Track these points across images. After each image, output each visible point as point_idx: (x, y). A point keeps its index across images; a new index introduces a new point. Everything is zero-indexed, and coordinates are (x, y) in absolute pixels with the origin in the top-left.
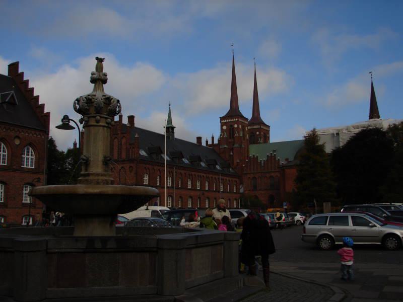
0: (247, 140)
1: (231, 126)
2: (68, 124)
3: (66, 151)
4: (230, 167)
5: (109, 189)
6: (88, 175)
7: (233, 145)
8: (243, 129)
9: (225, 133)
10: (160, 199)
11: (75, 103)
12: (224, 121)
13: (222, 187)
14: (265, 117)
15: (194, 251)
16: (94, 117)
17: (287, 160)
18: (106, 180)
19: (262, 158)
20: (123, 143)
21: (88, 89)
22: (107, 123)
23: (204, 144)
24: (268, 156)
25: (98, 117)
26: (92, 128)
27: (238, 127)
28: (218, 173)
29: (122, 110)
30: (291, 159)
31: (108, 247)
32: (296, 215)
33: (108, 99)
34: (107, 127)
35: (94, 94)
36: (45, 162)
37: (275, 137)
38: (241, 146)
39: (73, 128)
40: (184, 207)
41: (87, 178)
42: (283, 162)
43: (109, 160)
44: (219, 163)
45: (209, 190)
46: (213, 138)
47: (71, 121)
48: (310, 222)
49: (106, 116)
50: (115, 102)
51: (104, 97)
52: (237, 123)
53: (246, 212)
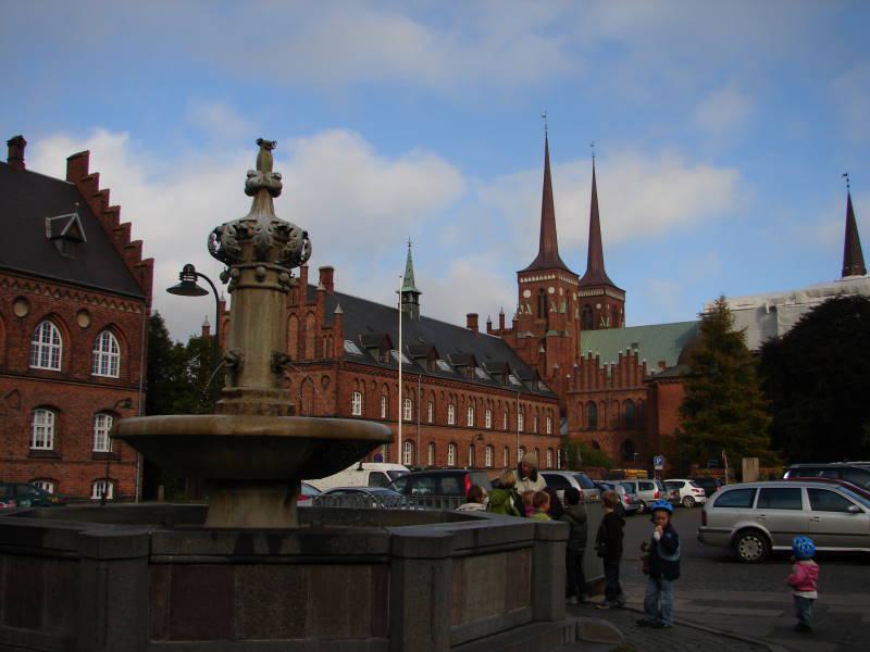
0: (576, 320)
2: (193, 283)
3: (186, 343)
4: (540, 379)
5: (285, 426)
6: (239, 394)
7: (547, 331)
8: (569, 299)
9: (528, 306)
11: (211, 238)
12: (526, 280)
13: (520, 421)
14: (614, 272)
15: (470, 563)
16: (254, 268)
17: (662, 364)
18: (278, 406)
19: (609, 361)
20: (308, 328)
21: (239, 207)
22: (280, 281)
23: (482, 329)
25: (262, 270)
26: (247, 291)
27: (557, 292)
28: (512, 392)
30: (672, 362)
31: (283, 552)
32: (682, 485)
33: (284, 231)
34: (280, 290)
35: (254, 218)
37: (636, 315)
38: (563, 332)
39: (206, 293)
40: (460, 466)
41: (235, 401)
42: (653, 369)
43: (284, 363)
44: (514, 371)
45: (492, 430)
46: (502, 317)
47: (199, 278)
48: (717, 501)
49: (279, 267)
50: (299, 237)
51: (275, 226)
52: (555, 283)
53: (574, 477)
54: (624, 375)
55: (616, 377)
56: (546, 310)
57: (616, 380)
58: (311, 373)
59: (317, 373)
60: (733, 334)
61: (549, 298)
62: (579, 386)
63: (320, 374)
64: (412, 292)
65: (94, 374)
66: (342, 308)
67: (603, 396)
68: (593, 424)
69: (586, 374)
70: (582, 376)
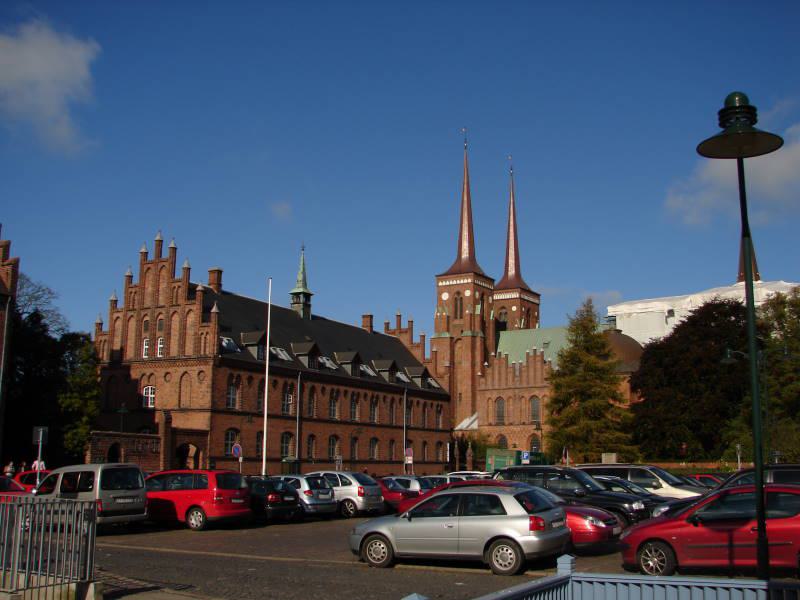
1: (458, 293)
12: (444, 283)
20: (188, 326)
24: (528, 354)
32: (347, 483)
48: (522, 494)
54: (532, 374)
56: (462, 311)
57: (524, 378)
59: (195, 368)
60: (599, 336)
61: (465, 302)
62: (489, 382)
63: (196, 369)
64: (303, 293)
65: (61, 368)
66: (219, 308)
67: (510, 393)
68: (500, 420)
69: (496, 372)
70: (493, 374)
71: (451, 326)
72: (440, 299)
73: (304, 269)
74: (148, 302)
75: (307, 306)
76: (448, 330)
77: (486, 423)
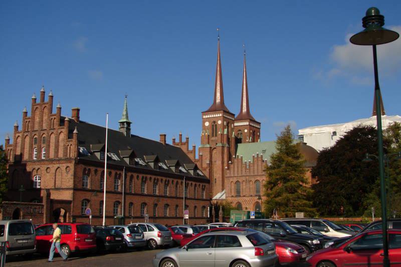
10: (197, 235)
12: (206, 117)
29: (22, 120)
32: (151, 230)
36: (88, 246)
46: (181, 135)
48: (249, 235)
54: (256, 167)
55: (252, 168)
58: (61, 165)
60: (294, 146)
63: (65, 165)
67: (244, 179)
68: (238, 194)
71: (210, 141)
72: (204, 125)
73: (127, 108)
74: (37, 127)
75: (128, 129)
76: (208, 143)
77: (230, 196)
